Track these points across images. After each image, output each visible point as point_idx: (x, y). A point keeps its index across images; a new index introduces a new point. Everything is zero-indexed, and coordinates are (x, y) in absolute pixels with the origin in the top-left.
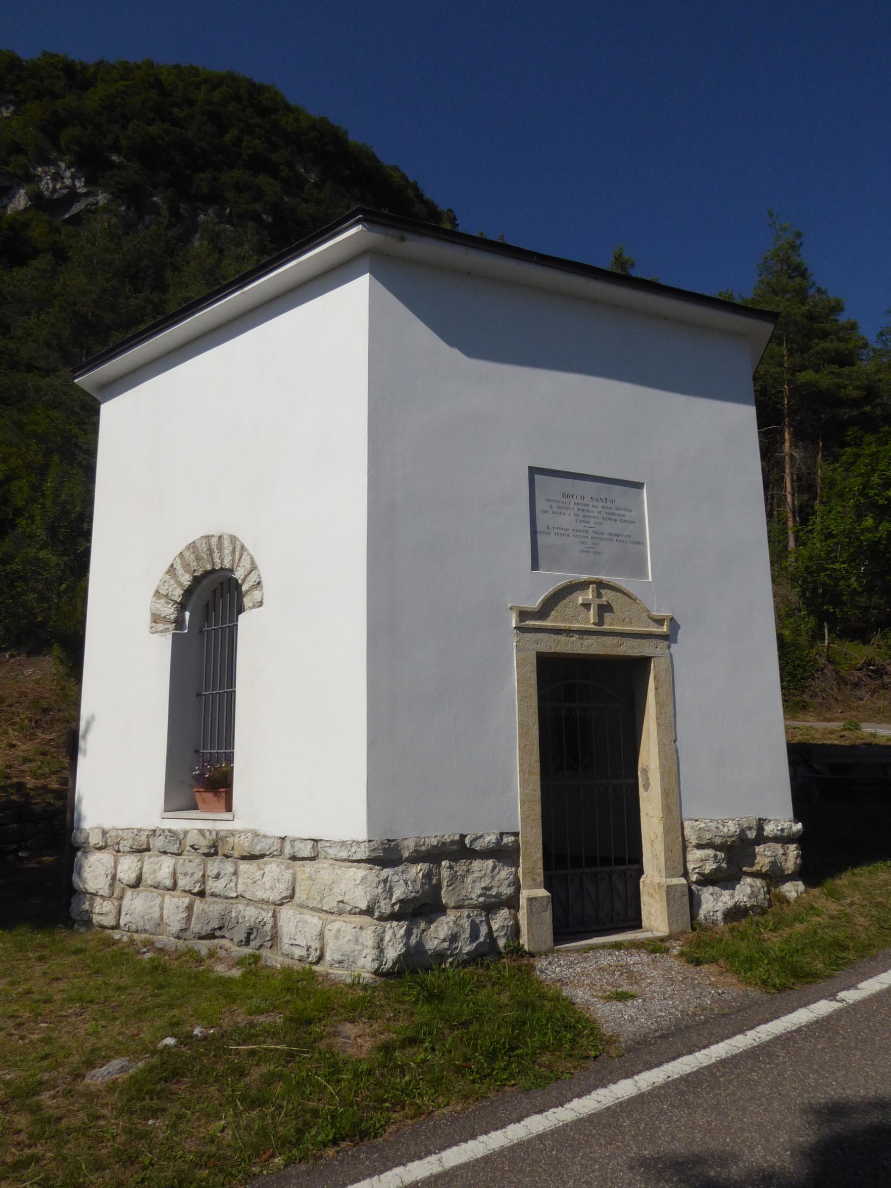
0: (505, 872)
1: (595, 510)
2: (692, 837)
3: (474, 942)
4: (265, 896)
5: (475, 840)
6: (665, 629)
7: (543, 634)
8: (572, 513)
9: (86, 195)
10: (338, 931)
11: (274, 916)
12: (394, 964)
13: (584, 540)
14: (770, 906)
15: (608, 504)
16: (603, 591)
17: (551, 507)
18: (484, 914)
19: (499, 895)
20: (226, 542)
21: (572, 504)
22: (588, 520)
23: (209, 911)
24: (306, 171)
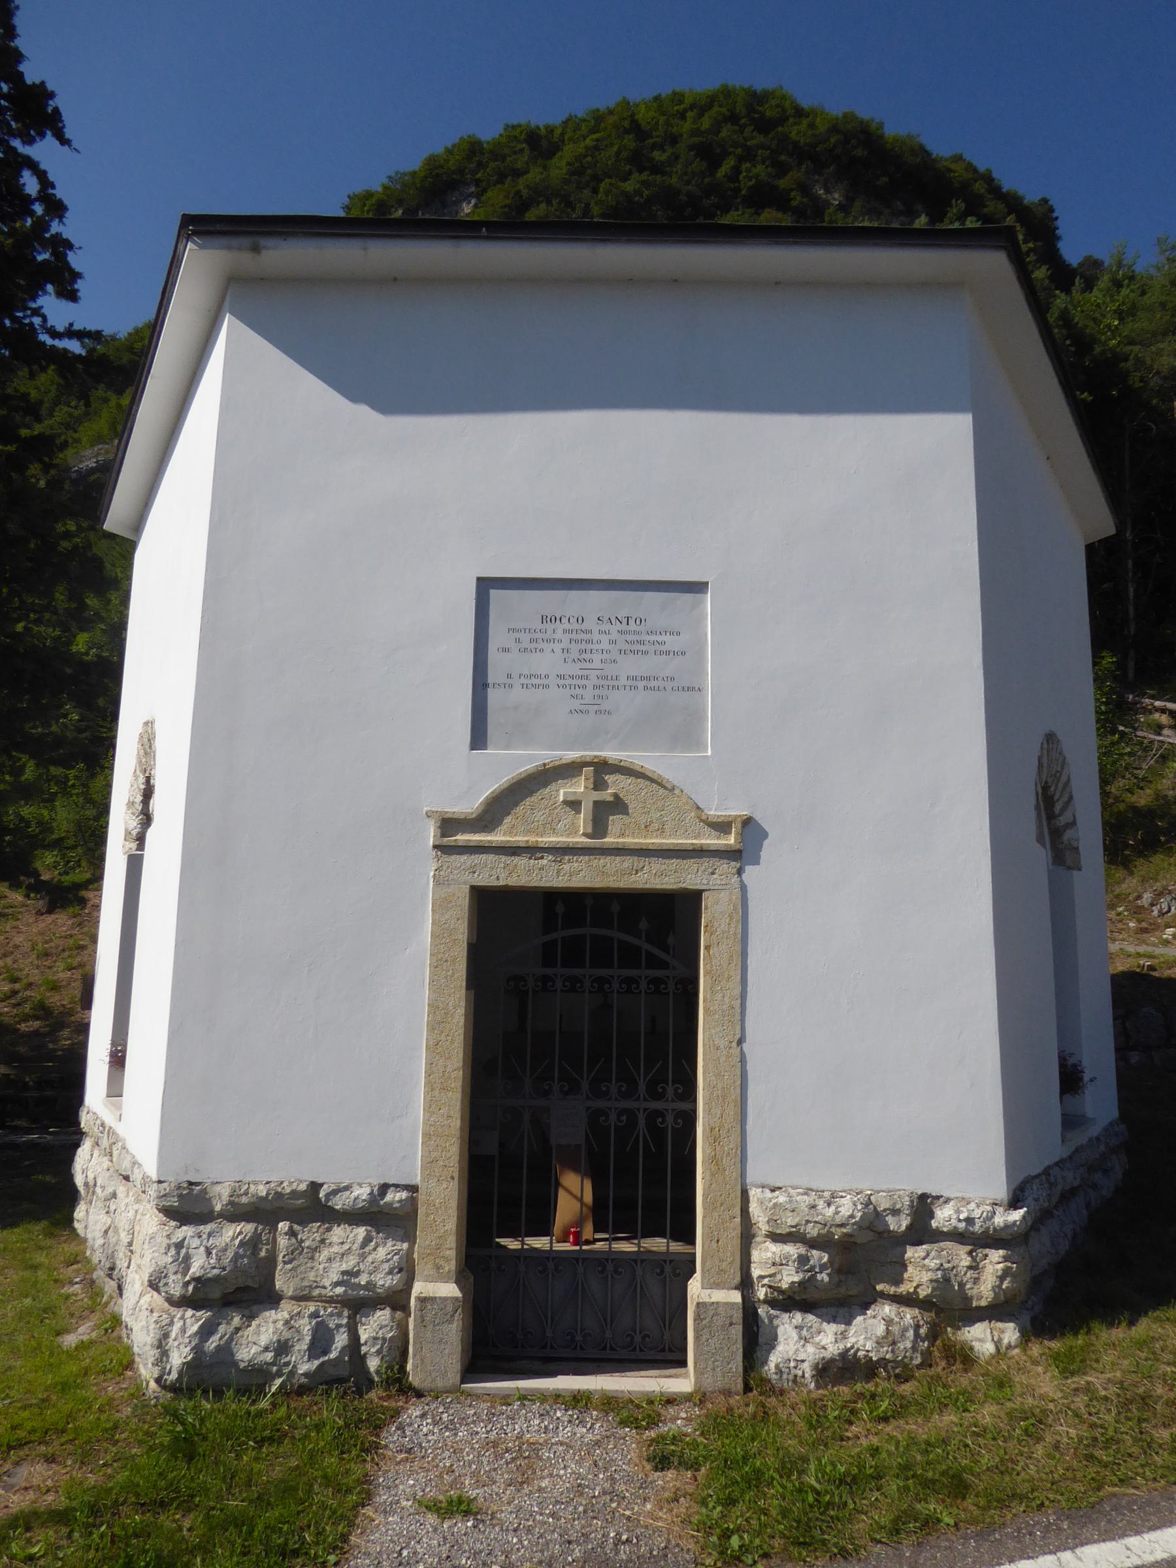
0: (386, 1251)
1: (605, 638)
3: (317, 1358)
5: (335, 1192)
6: (731, 840)
7: (484, 856)
8: (557, 647)
12: (180, 1373)
14: (927, 1363)
15: (633, 626)
16: (610, 778)
17: (518, 641)
18: (346, 1313)
19: (370, 1286)
22: (588, 656)
24: (827, 191)
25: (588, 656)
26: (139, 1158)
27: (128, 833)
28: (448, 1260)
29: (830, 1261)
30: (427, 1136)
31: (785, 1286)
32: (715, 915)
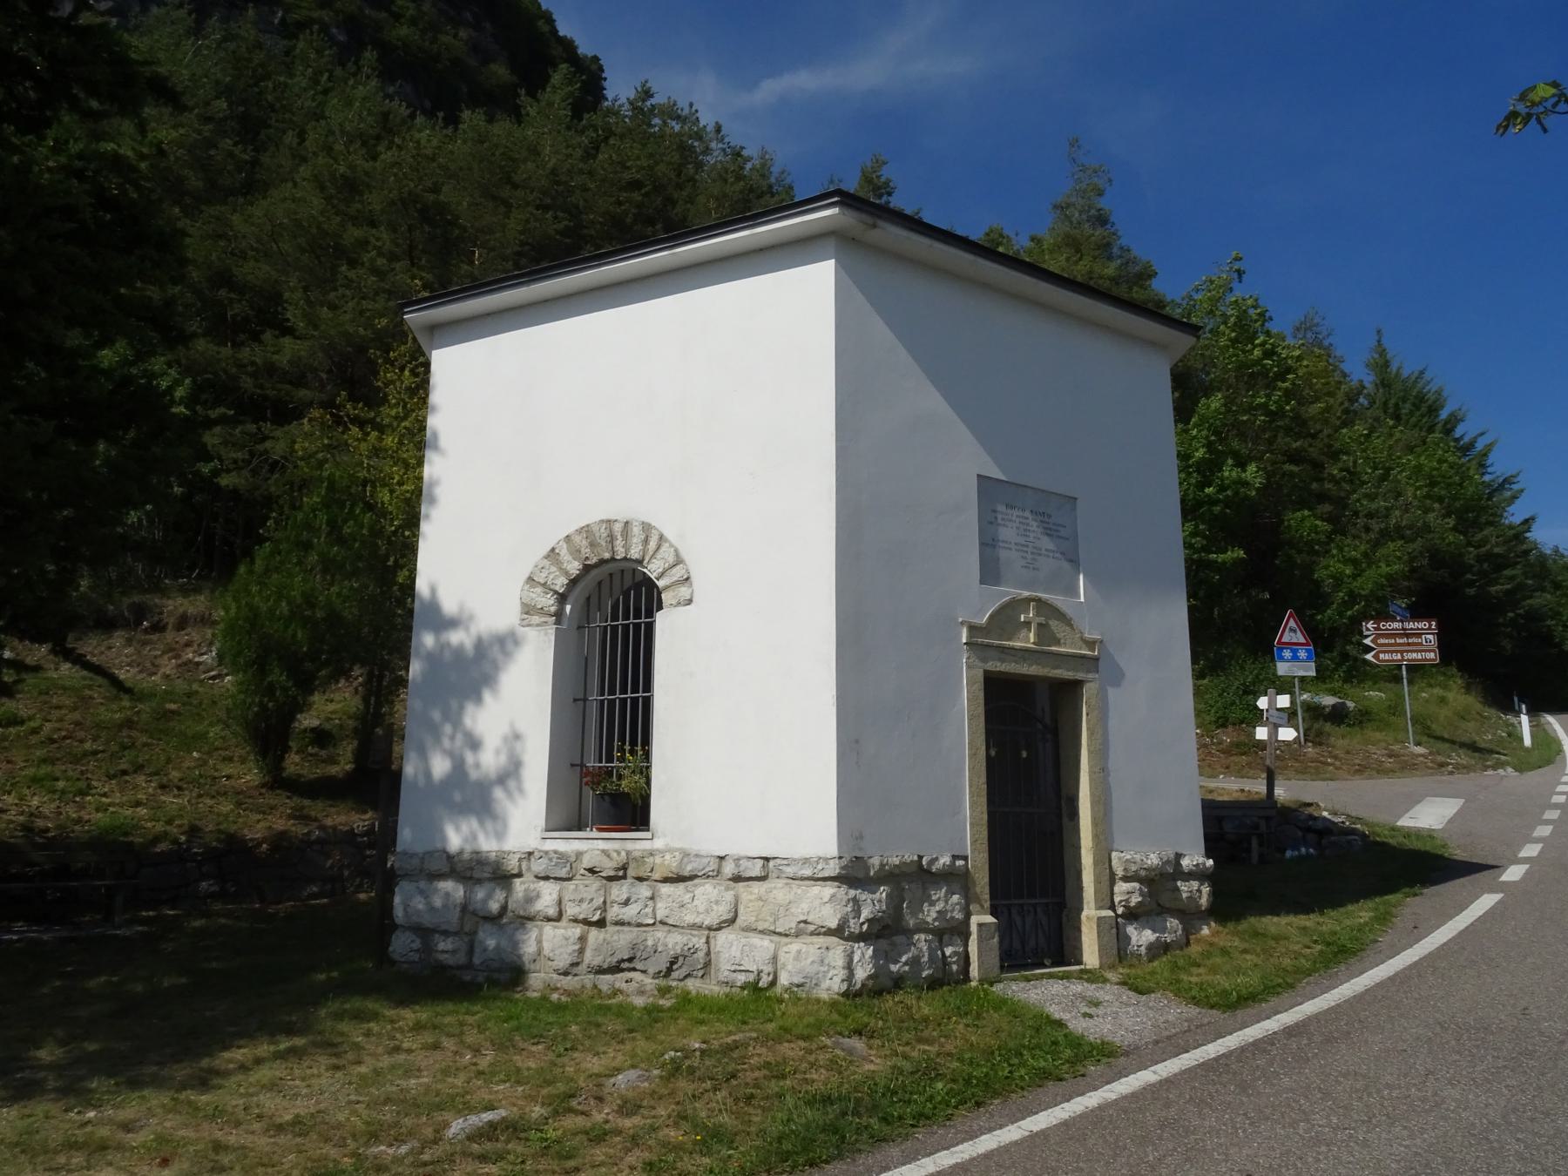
2: (1120, 872)
4: (698, 920)
10: (799, 952)
11: (707, 942)
20: (636, 530)
23: (620, 941)
32: (1088, 691)
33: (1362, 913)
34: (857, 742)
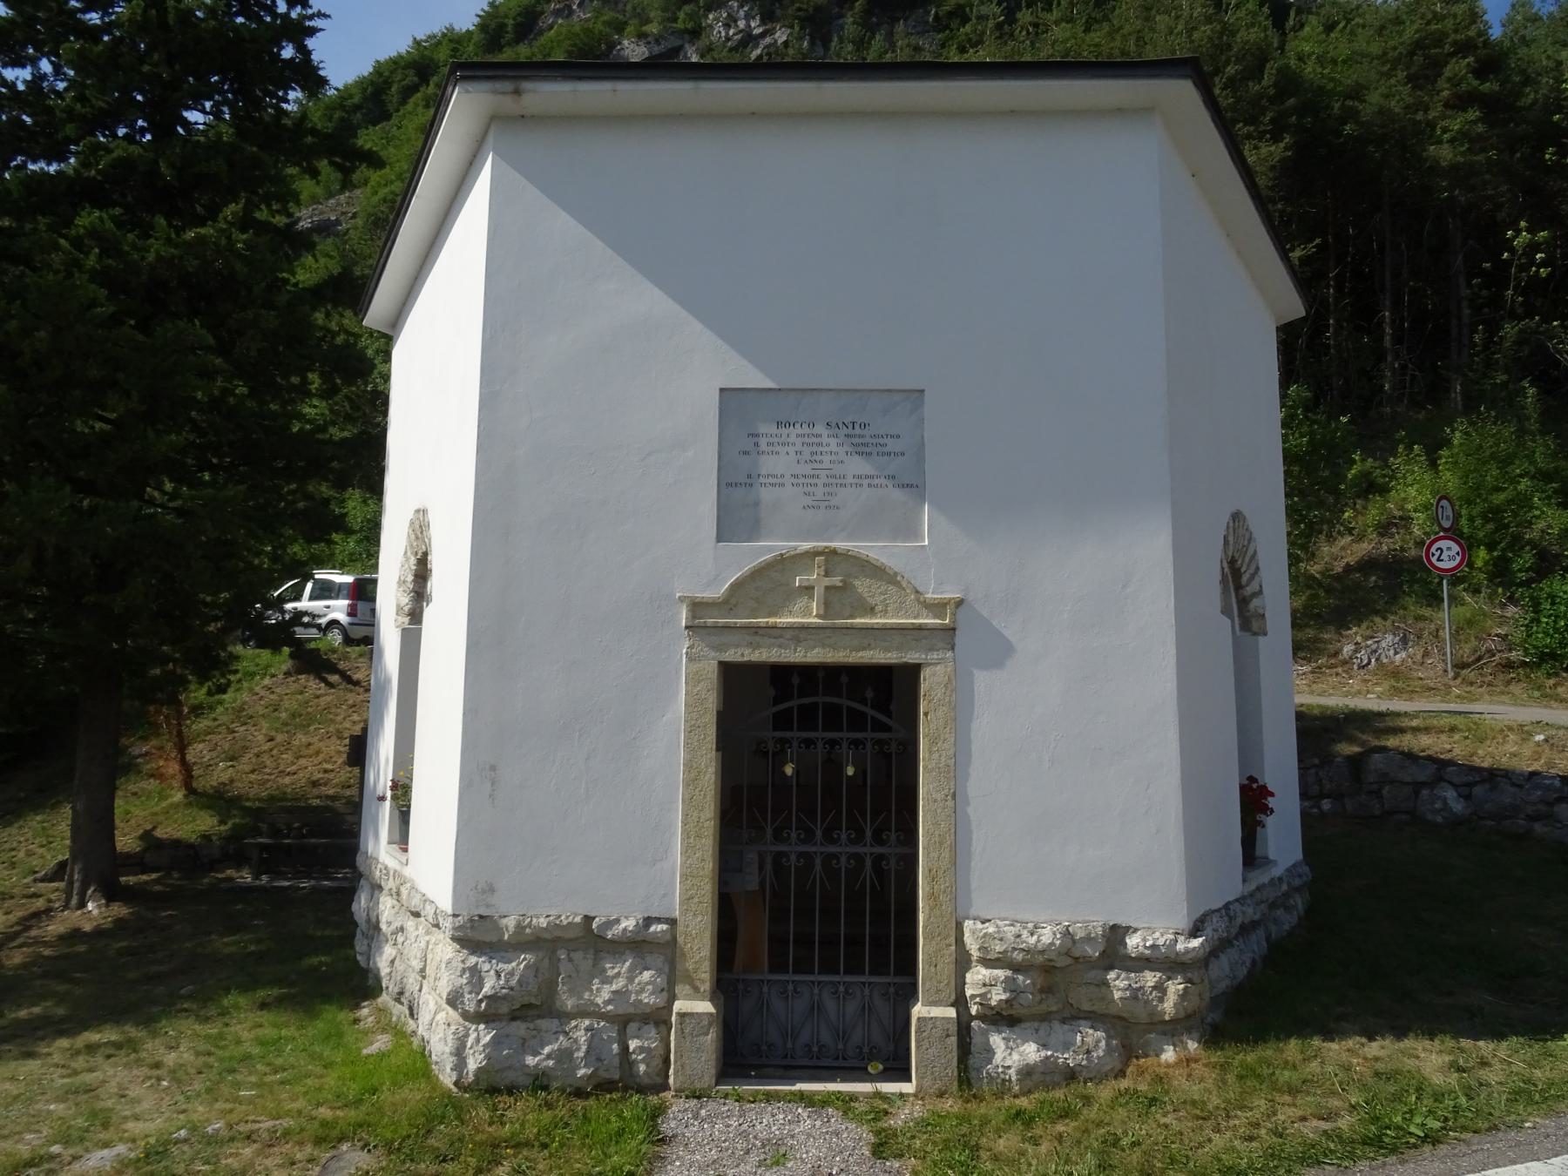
2: (975, 954)
8: (791, 450)
9: (763, 35)
13: (810, 489)
15: (858, 431)
21: (793, 437)
22: (818, 458)
25: (818, 458)
26: (430, 896)
27: (399, 609)
28: (703, 981)
29: (1033, 984)
30: (684, 877)
31: (993, 1003)
32: (931, 683)
33: (1503, 1060)
34: (493, 768)
